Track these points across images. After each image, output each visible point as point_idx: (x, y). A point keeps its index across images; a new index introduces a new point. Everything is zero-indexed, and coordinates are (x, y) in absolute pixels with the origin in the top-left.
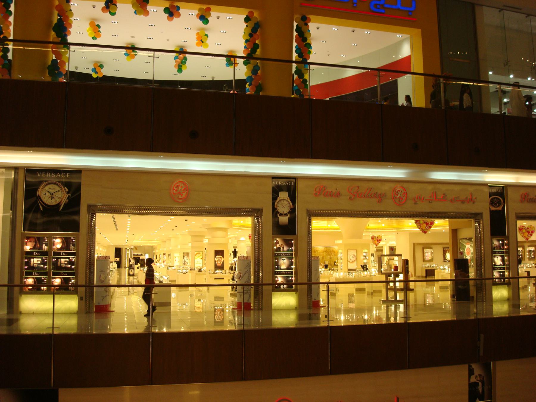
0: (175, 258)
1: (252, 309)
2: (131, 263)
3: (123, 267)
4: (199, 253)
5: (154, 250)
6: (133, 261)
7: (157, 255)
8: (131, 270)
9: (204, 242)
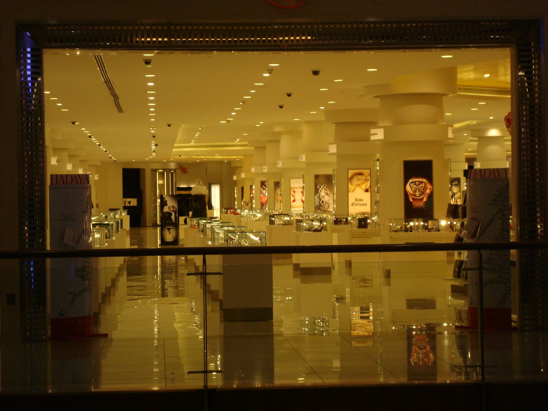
0: (292, 193)
1: (515, 329)
2: (166, 209)
3: (149, 222)
4: (361, 174)
5: (234, 174)
6: (171, 204)
7: (242, 189)
8: (169, 229)
9: (373, 138)
